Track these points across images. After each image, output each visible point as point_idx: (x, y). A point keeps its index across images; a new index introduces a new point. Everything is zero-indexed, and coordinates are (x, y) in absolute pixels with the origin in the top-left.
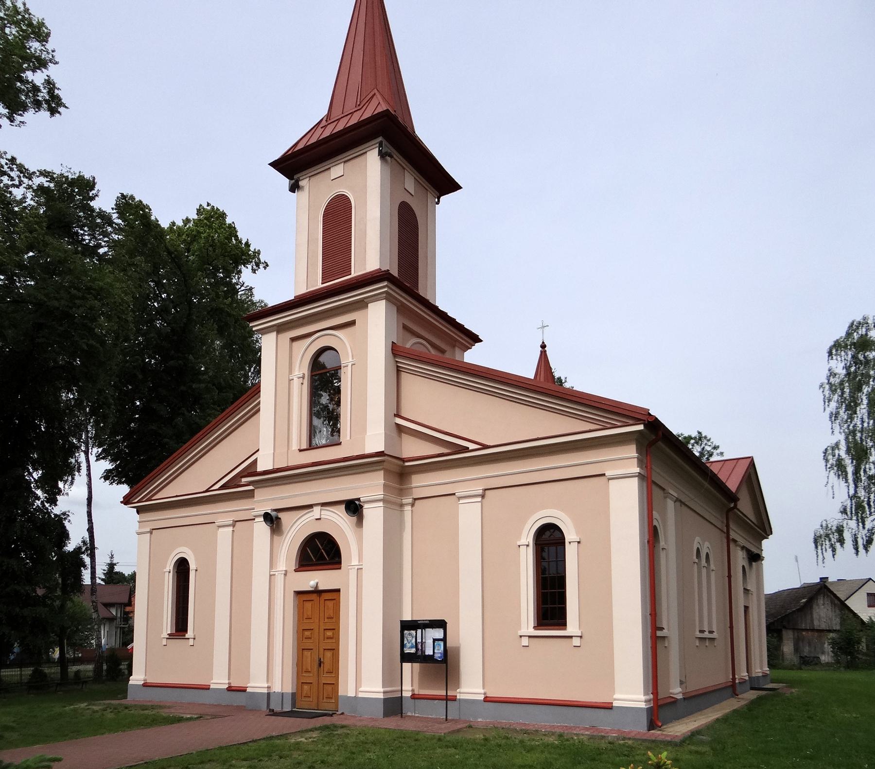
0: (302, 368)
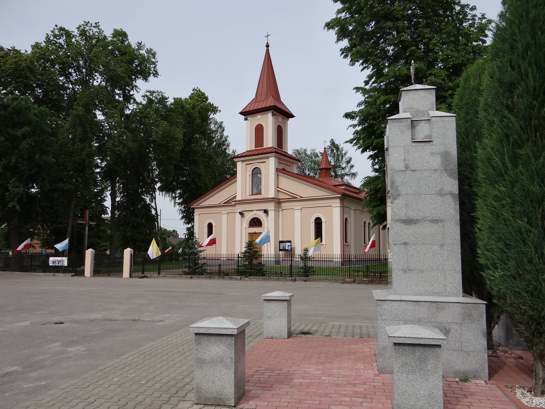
0: (249, 173)
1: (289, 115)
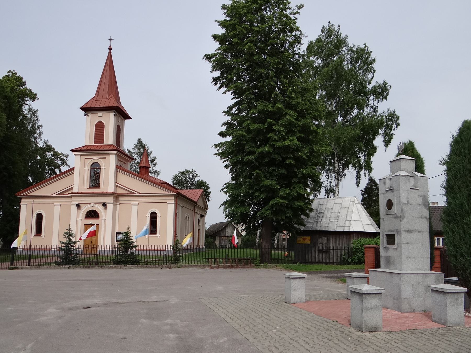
0: (88, 167)
1: (128, 117)
